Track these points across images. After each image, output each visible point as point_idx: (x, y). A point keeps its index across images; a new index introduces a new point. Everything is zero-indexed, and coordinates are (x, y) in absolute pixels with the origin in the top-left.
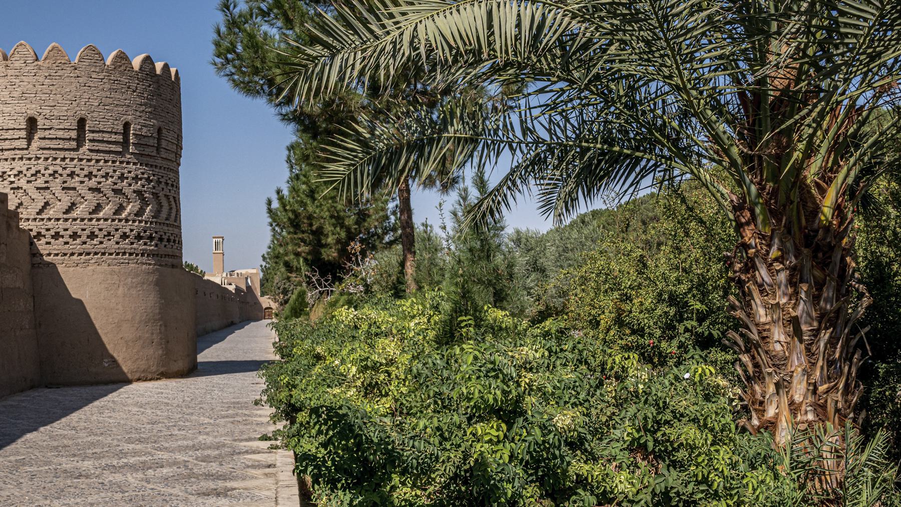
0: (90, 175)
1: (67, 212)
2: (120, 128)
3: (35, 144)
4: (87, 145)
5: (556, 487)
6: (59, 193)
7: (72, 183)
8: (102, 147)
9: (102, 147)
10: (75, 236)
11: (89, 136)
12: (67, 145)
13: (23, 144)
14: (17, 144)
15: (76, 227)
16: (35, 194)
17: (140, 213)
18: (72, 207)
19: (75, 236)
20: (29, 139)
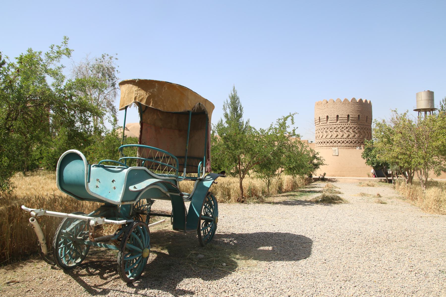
0: (335, 128)
1: (342, 136)
2: (347, 116)
3: (328, 122)
4: (338, 121)
5: (2, 153)
6: (352, 132)
7: (332, 130)
8: (342, 121)
9: (342, 121)
10: (343, 142)
11: (350, 119)
12: (334, 121)
13: (346, 121)
14: (324, 122)
15: (339, 140)
16: (335, 132)
17: (354, 136)
18: (349, 135)
19: (347, 142)
20: (327, 120)
